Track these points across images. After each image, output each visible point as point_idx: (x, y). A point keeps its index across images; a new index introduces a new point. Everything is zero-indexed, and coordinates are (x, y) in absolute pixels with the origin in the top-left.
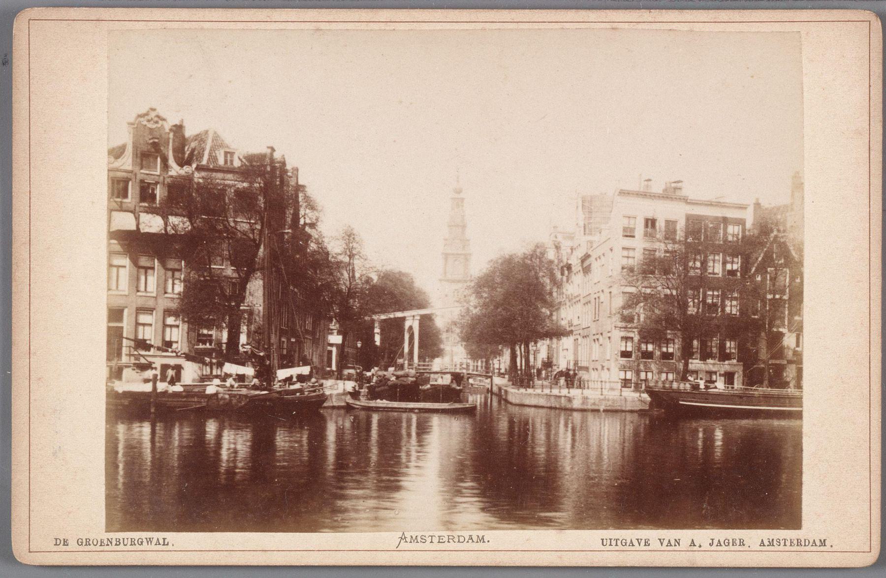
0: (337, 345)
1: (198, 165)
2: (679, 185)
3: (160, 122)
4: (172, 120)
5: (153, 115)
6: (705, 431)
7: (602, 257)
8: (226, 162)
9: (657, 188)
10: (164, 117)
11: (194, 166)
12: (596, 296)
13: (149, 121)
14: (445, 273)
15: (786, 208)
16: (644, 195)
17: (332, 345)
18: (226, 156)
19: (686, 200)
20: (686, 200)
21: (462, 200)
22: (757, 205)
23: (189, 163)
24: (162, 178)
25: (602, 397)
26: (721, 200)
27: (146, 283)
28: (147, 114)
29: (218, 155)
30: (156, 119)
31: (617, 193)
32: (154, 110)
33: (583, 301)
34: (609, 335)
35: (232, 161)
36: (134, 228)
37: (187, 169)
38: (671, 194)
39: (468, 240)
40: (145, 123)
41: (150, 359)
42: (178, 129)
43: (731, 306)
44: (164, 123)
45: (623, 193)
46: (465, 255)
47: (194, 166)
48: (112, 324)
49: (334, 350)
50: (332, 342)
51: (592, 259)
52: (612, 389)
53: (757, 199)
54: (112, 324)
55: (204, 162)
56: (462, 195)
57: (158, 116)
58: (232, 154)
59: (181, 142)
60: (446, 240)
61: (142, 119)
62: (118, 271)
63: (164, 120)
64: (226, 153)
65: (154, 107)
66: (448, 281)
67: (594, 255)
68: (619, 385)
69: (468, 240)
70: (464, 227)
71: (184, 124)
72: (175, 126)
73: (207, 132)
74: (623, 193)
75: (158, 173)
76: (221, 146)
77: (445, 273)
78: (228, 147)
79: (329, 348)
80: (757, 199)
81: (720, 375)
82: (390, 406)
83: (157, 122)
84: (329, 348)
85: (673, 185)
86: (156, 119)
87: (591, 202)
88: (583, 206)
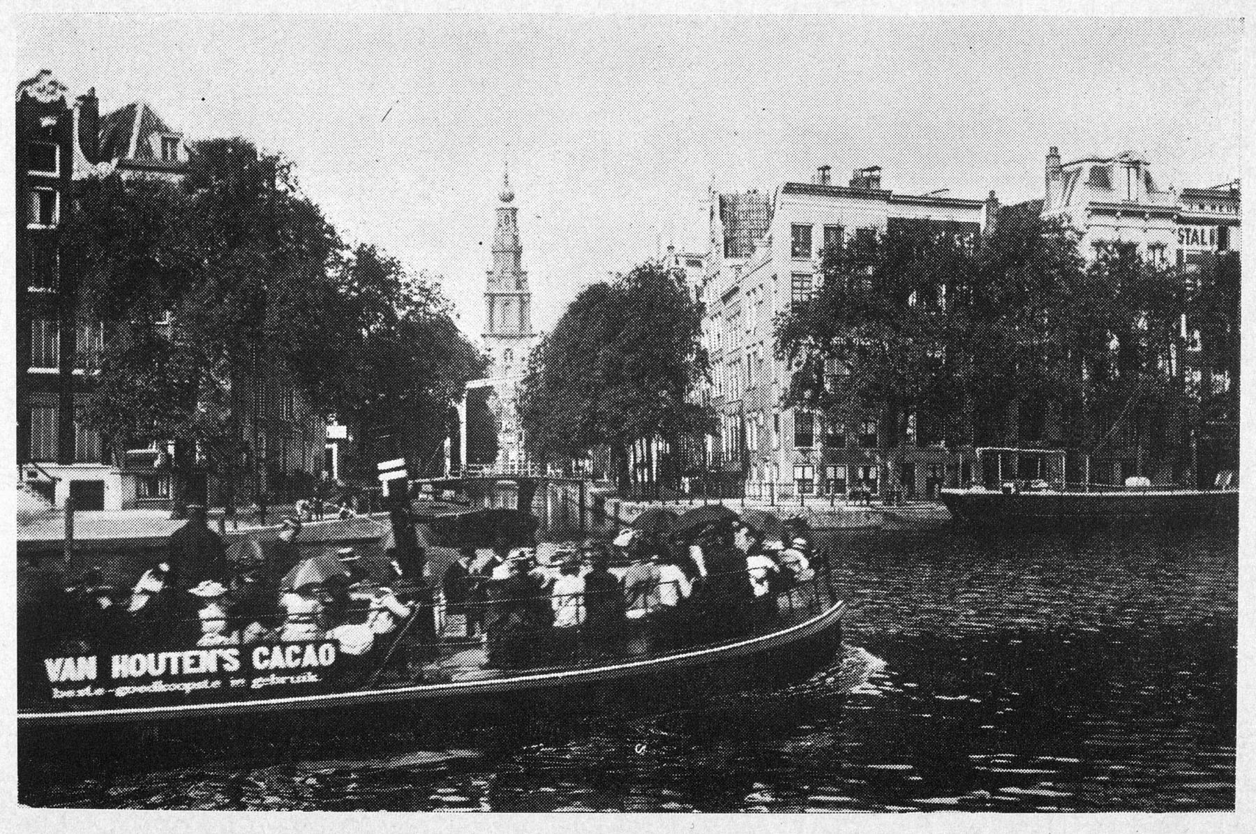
0: (338, 441)
1: (120, 161)
2: (876, 173)
3: (59, 93)
7: (758, 290)
8: (165, 153)
9: (841, 179)
12: (750, 351)
13: (39, 90)
14: (492, 326)
15: (1040, 203)
16: (821, 189)
17: (331, 441)
18: (164, 146)
19: (887, 197)
20: (887, 197)
21: (514, 211)
26: (943, 195)
27: (1071, 164)
28: (36, 80)
31: (781, 189)
32: (48, 72)
33: (727, 360)
35: (174, 155)
37: (104, 169)
38: (865, 187)
39: (525, 273)
42: (89, 102)
45: (790, 188)
46: (521, 296)
47: (115, 161)
48: (22, 716)
49: (334, 447)
50: (332, 436)
51: (741, 294)
53: (992, 193)
54: (22, 716)
55: (130, 155)
58: (175, 141)
60: (490, 273)
61: (28, 88)
63: (64, 89)
64: (164, 140)
65: (46, 68)
66: (495, 336)
70: (518, 253)
71: (97, 95)
73: (132, 108)
74: (790, 188)
76: (159, 127)
77: (492, 326)
78: (167, 130)
79: (327, 446)
83: (53, 93)
84: (327, 446)
85: (866, 174)
86: (51, 88)
87: (733, 205)
88: (722, 212)
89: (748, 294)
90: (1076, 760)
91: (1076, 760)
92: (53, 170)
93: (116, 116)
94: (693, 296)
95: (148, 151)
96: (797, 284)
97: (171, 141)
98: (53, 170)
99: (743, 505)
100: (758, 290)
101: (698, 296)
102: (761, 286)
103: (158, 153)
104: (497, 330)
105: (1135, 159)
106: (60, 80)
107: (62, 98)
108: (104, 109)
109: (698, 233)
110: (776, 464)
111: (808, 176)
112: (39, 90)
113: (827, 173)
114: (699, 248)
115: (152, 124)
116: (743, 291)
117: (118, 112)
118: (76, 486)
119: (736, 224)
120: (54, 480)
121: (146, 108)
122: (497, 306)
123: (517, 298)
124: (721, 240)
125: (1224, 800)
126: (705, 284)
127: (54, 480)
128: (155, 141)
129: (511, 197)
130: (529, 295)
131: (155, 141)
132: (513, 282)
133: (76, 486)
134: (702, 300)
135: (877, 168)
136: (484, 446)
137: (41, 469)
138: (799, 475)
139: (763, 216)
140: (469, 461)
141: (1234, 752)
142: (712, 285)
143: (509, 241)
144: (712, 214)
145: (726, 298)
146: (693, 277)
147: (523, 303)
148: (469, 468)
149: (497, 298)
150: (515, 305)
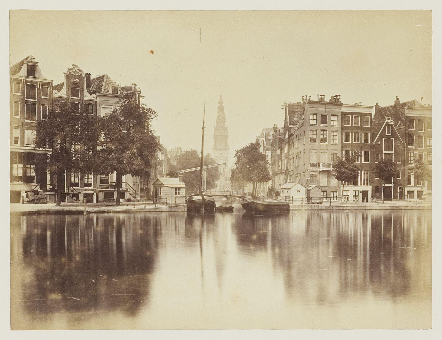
2: (338, 97)
3: (80, 72)
4: (86, 72)
5: (76, 69)
9: (327, 99)
10: (82, 70)
11: (97, 94)
13: (74, 72)
22: (377, 105)
23: (94, 93)
30: (78, 71)
40: (72, 73)
41: (78, 191)
42: (88, 75)
43: (75, 177)
45: (310, 102)
53: (377, 104)
55: (102, 92)
56: (223, 105)
57: (78, 69)
59: (89, 82)
61: (71, 71)
62: (54, 195)
69: (227, 128)
80: (377, 104)
81: (360, 192)
82: (359, 249)
83: (78, 73)
85: (335, 97)
86: (78, 71)
90: (421, 25)
91: (421, 25)
93: (97, 79)
95: (108, 91)
100: (300, 135)
102: (300, 134)
103: (110, 92)
105: (21, 124)
106: (80, 68)
107: (81, 74)
108: (92, 77)
111: (315, 98)
112: (74, 72)
116: (295, 135)
121: (107, 77)
129: (223, 103)
135: (323, 95)
139: (302, 110)
141: (431, 115)
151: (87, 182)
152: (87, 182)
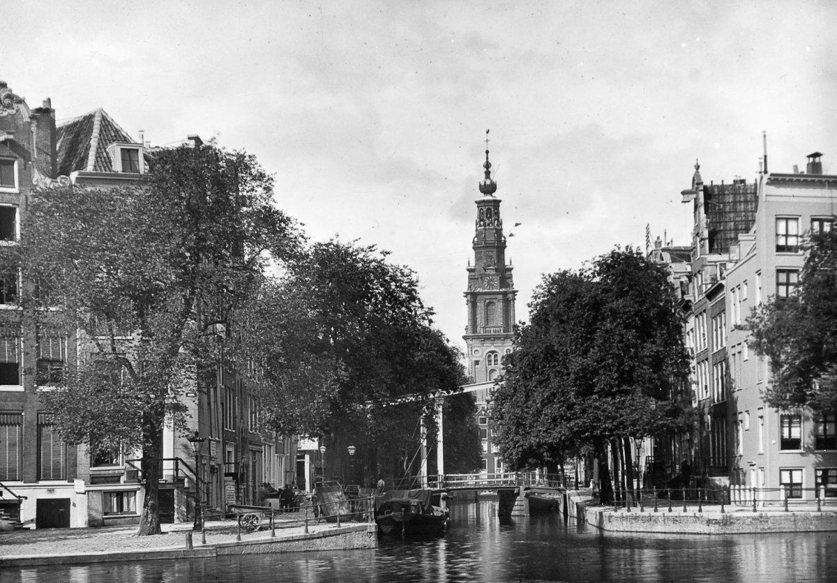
3: (15, 106)
6: (624, 439)
10: (21, 96)
21: (497, 203)
24: (22, 198)
25: (756, 514)
29: (111, 155)
34: (760, 413)
36: (164, 457)
42: (45, 113)
44: (21, 106)
45: (778, 180)
46: (505, 294)
52: (771, 502)
55: (90, 168)
56: (497, 195)
63: (21, 101)
66: (478, 338)
67: (728, 283)
68: (782, 495)
69: (511, 269)
71: (53, 106)
72: (39, 110)
73: (89, 118)
75: (16, 190)
76: (119, 137)
83: (9, 106)
86: (7, 101)
88: (706, 204)
89: (733, 290)
92: (12, 184)
94: (679, 293)
95: (108, 162)
96: (783, 278)
97: (129, 155)
98: (12, 184)
99: (723, 511)
101: (683, 293)
103: (117, 166)
104: (481, 331)
109: (681, 226)
110: (762, 469)
113: (817, 160)
114: (684, 240)
115: (110, 133)
117: (75, 124)
118: (41, 504)
119: (725, 211)
120: (20, 500)
121: (104, 119)
122: (481, 306)
123: (500, 297)
124: (706, 234)
125: (38, 500)
126: (690, 281)
127: (20, 500)
128: (115, 151)
130: (514, 293)
131: (115, 151)
132: (497, 282)
133: (41, 504)
134: (687, 298)
136: (708, 427)
137: (6, 487)
138: (786, 480)
140: (445, 472)
142: (698, 281)
143: (491, 238)
144: (696, 207)
145: (711, 295)
146: (677, 272)
147: (769, 196)
148: (446, 478)
149: (479, 297)
150: (499, 306)
151: (785, 295)
152: (785, 295)
